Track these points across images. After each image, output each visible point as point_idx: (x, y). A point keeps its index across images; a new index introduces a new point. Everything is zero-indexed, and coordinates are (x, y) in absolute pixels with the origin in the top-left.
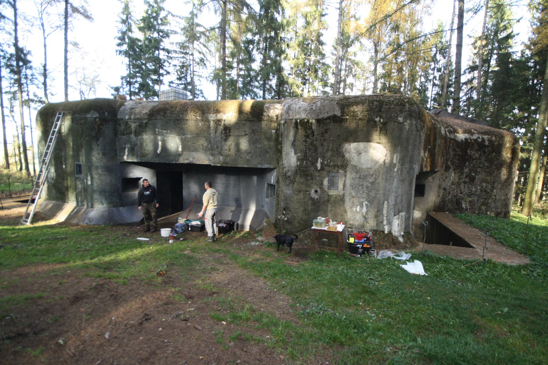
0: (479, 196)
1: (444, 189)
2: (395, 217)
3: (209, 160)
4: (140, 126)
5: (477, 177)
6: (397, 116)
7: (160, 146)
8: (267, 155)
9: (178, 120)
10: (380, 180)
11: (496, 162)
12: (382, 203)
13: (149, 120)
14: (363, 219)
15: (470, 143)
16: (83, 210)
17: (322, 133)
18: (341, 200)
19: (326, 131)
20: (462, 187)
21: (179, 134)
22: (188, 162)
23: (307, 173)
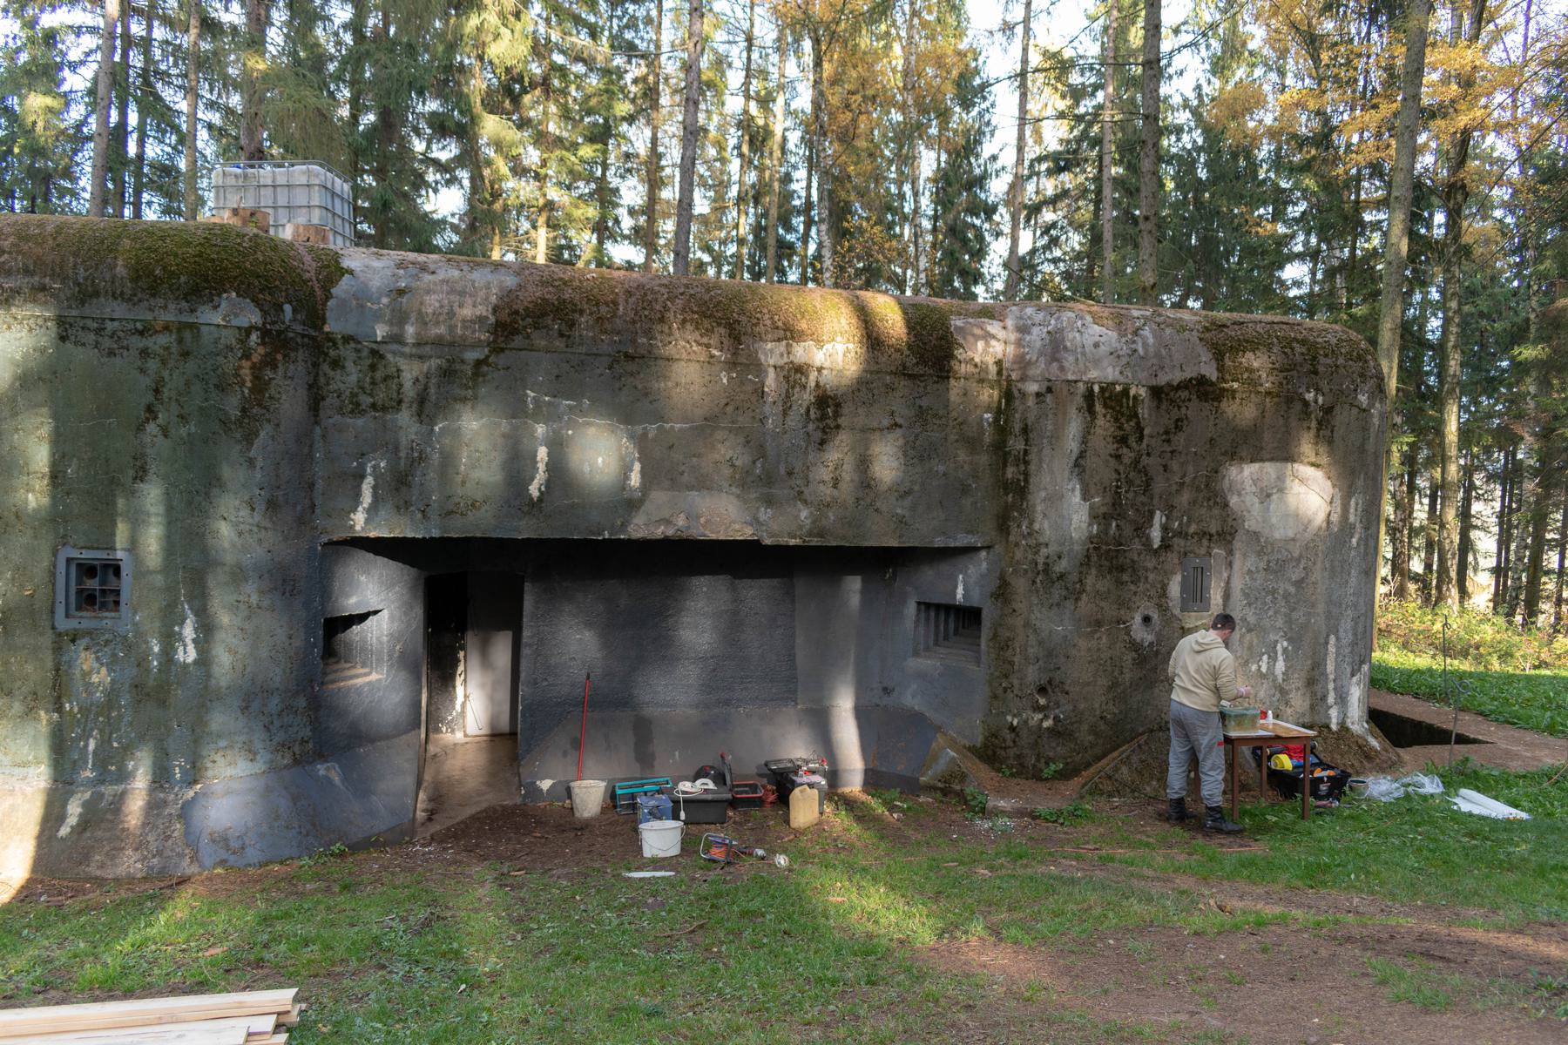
2: (1355, 679)
3: (756, 521)
6: (1355, 390)
7: (541, 467)
8: (967, 502)
9: (629, 357)
10: (1317, 575)
12: (1322, 641)
14: (1278, 695)
17: (1167, 433)
19: (1178, 425)
22: (670, 532)
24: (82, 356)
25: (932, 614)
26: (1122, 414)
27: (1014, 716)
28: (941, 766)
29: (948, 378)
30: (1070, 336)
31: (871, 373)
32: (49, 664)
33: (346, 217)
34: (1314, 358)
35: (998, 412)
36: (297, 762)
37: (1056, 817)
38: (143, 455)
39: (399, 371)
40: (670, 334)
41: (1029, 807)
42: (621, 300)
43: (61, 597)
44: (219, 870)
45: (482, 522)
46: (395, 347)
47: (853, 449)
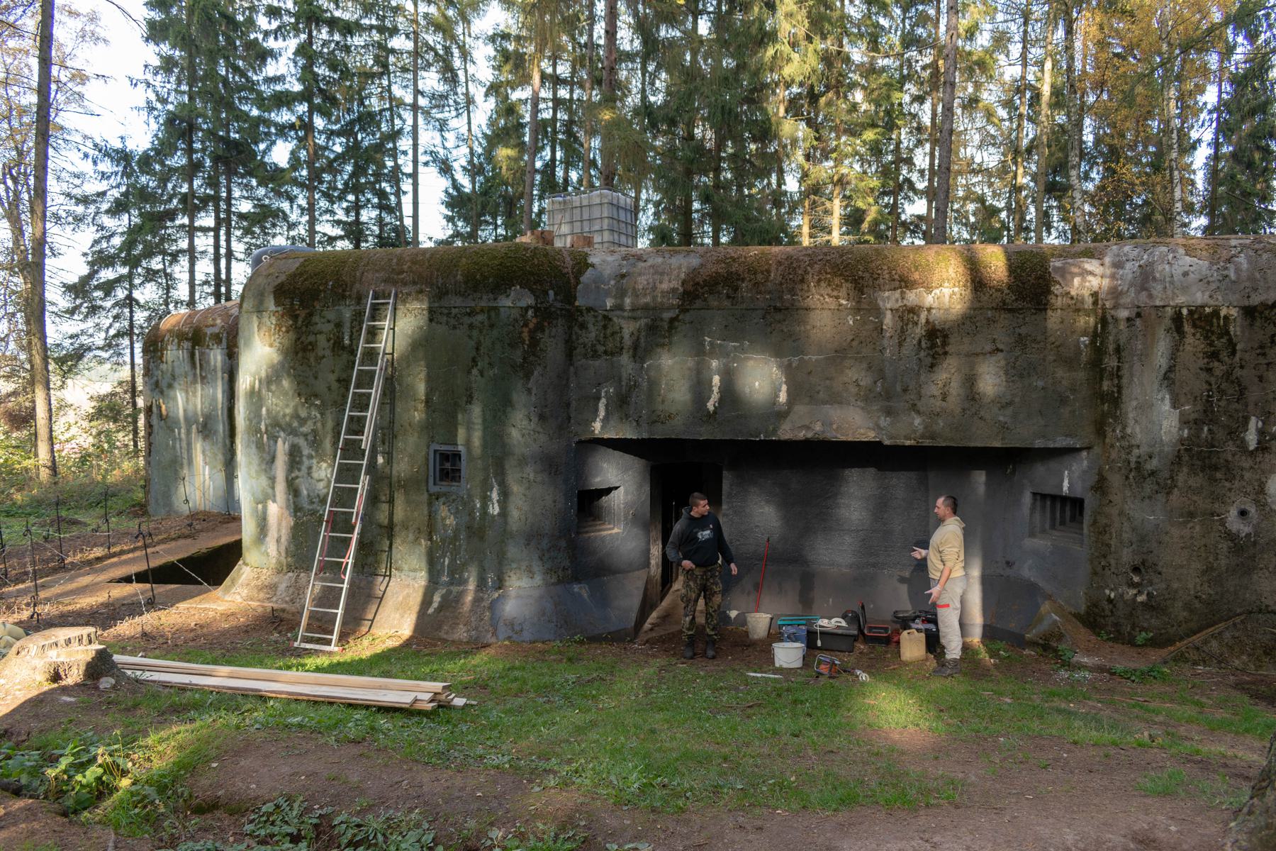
3: (878, 427)
4: (652, 328)
7: (716, 389)
8: (1065, 411)
9: (777, 310)
13: (684, 310)
16: (469, 598)
17: (1261, 347)
21: (778, 353)
22: (810, 435)
23: (1214, 460)
24: (441, 329)
25: (1058, 506)
26: (1213, 333)
27: (1112, 590)
28: (1044, 627)
29: (1046, 310)
30: (1160, 268)
31: (975, 309)
32: (426, 512)
33: (629, 221)
35: (1095, 335)
36: (559, 582)
37: (1126, 675)
38: (471, 388)
39: (621, 328)
40: (808, 291)
41: (1108, 665)
42: (773, 269)
43: (431, 473)
44: (507, 643)
45: (677, 428)
46: (618, 313)
47: (959, 370)
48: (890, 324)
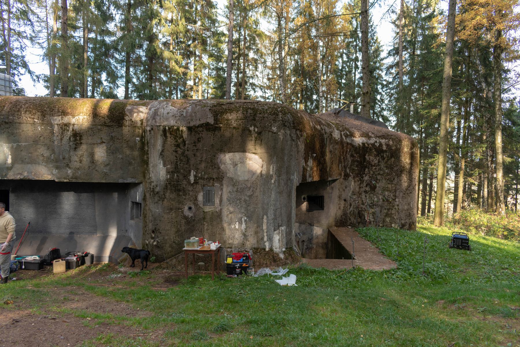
0: (382, 207)
1: (345, 200)
2: (276, 232)
5: (378, 185)
6: (271, 126)
8: (131, 168)
10: (257, 193)
11: (395, 169)
12: (261, 218)
14: (243, 237)
15: (367, 148)
17: (195, 143)
18: (218, 217)
19: (199, 140)
20: (363, 197)
22: (22, 177)
26: (177, 137)
29: (122, 126)
30: (160, 111)
34: (255, 115)
48: (57, 130)
